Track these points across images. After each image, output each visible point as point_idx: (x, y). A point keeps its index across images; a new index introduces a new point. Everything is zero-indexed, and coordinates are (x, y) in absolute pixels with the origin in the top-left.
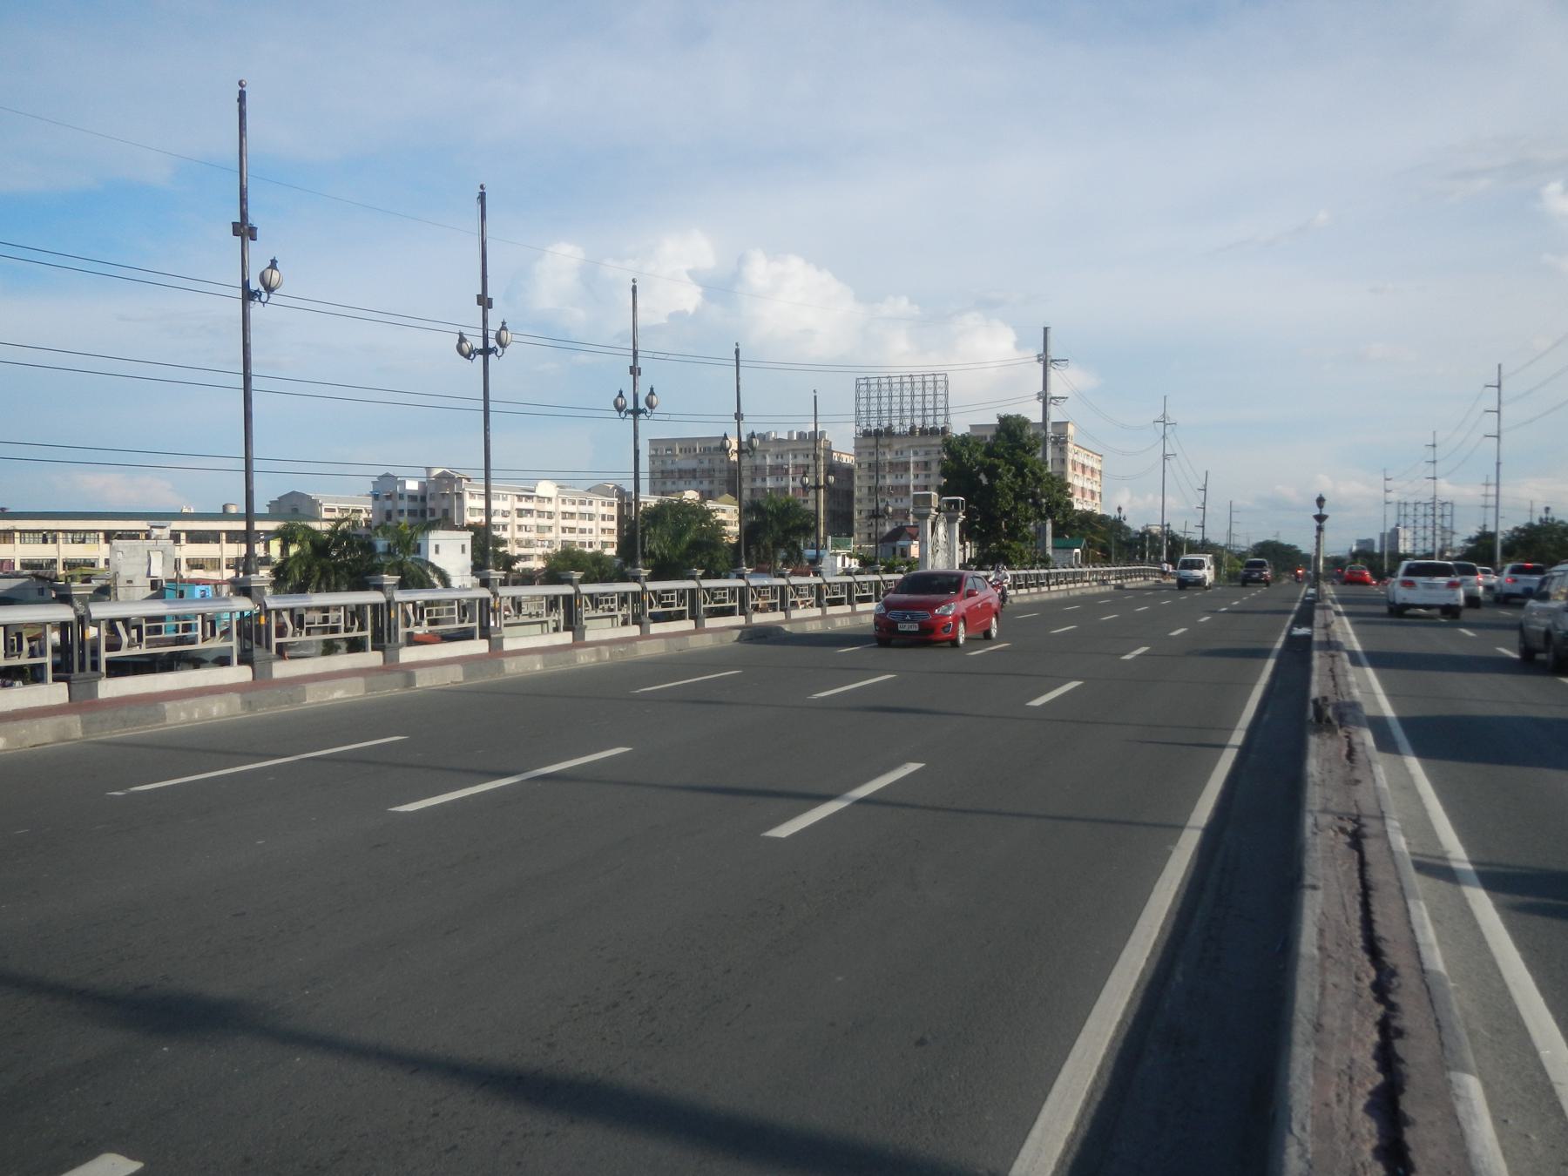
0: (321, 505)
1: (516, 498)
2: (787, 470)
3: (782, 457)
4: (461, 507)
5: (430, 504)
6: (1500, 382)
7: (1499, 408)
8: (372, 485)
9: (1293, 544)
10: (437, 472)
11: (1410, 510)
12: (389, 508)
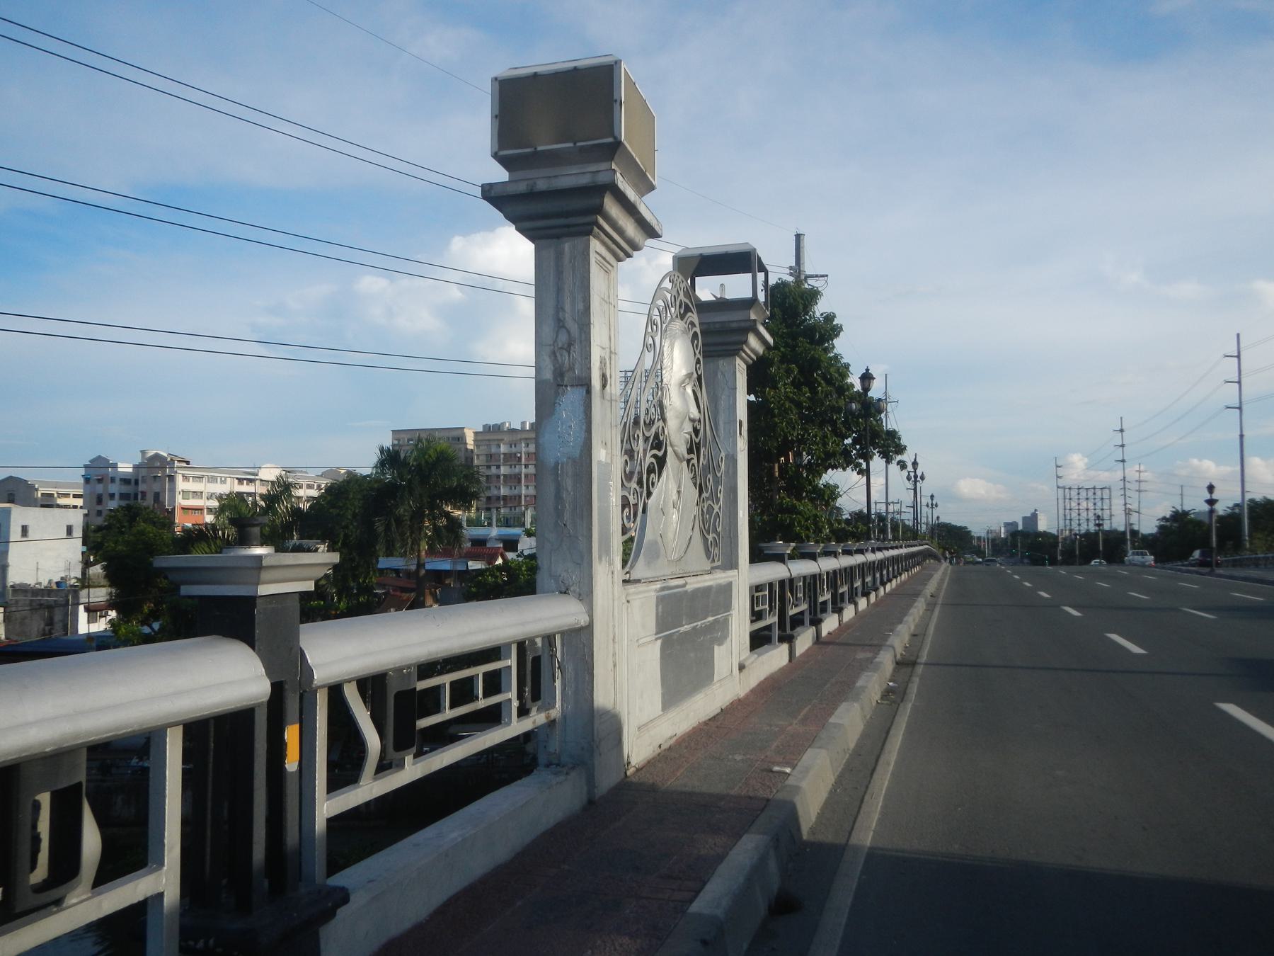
0: (37, 490)
1: (236, 481)
2: (520, 459)
3: (515, 446)
4: (173, 490)
5: (142, 487)
6: (1239, 352)
7: (1240, 378)
9: (963, 525)
10: (151, 454)
11: (1074, 493)
12: (101, 492)
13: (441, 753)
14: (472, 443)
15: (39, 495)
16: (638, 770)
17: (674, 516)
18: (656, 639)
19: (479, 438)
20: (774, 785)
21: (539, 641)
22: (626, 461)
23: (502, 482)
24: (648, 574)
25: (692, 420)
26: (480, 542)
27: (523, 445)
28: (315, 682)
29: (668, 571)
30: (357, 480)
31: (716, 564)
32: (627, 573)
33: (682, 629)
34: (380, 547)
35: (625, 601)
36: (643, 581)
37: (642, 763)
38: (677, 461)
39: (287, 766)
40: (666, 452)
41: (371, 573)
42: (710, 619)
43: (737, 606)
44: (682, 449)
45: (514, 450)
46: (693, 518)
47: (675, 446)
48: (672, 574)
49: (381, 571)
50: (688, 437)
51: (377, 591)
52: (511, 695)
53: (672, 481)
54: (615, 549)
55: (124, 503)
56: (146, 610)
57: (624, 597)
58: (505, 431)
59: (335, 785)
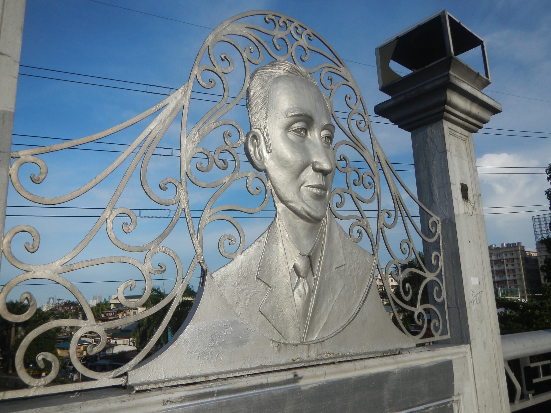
2: (503, 262)
3: (500, 256)
9: (497, 317)
23: (495, 274)
27: (504, 255)
41: (407, 322)
45: (499, 258)
47: (290, 202)
58: (493, 249)
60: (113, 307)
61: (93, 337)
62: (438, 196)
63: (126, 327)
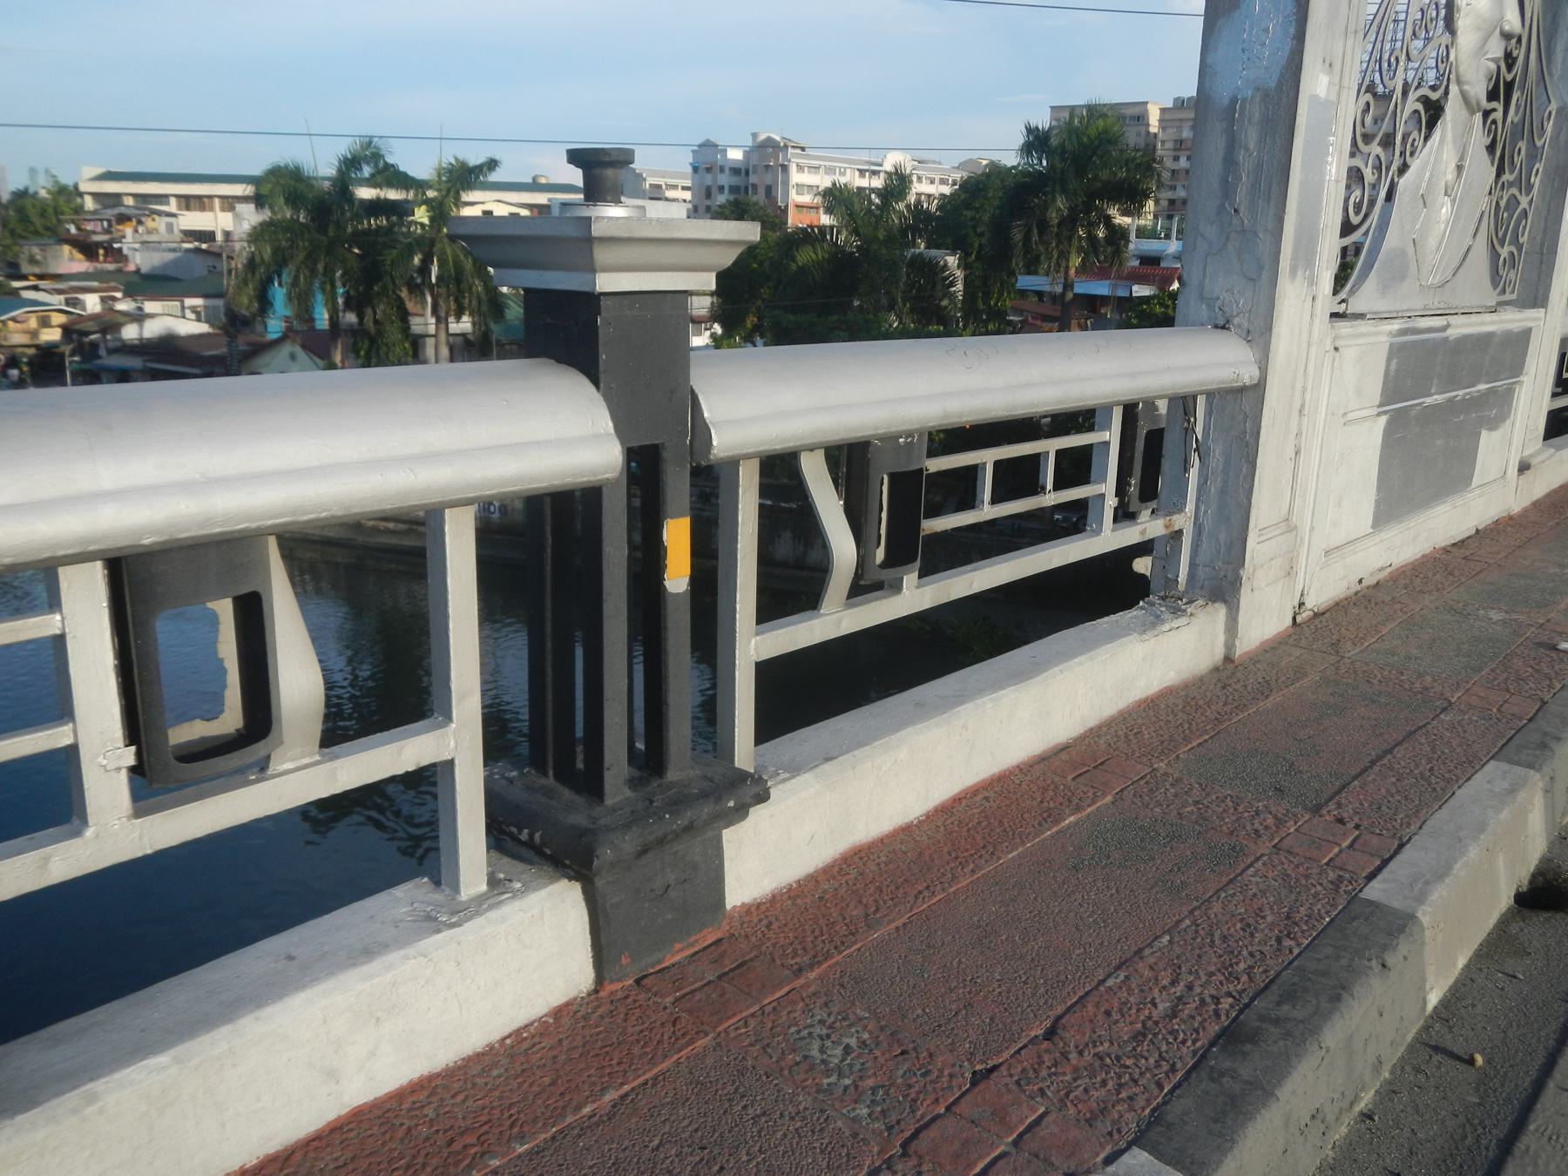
0: (645, 180)
1: (857, 173)
4: (786, 183)
5: (753, 179)
8: (691, 155)
10: (762, 137)
13: (971, 571)
14: (1157, 124)
15: (647, 186)
16: (1316, 615)
17: (1444, 210)
18: (1379, 414)
19: (1167, 117)
20: (1556, 673)
21: (1162, 406)
22: (1368, 104)
24: (1382, 306)
25: (1507, 36)
26: (1151, 261)
28: (715, 451)
29: (1417, 304)
30: (1000, 173)
31: (1508, 297)
32: (1343, 301)
33: (1429, 401)
34: (1017, 262)
35: (1329, 347)
36: (1368, 316)
37: (1326, 604)
38: (1464, 113)
39: (667, 583)
40: (1447, 92)
42: (1482, 387)
43: (1533, 371)
44: (1479, 90)
46: (1478, 215)
48: (1425, 309)
49: (1023, 293)
50: (1493, 66)
51: (1011, 318)
52: (1104, 488)
53: (1450, 146)
54: (1325, 258)
55: (731, 198)
56: (749, 325)
57: (1329, 341)
59: (772, 607)
60: (89, 204)
61: (59, 292)
62: (1559, 66)
63: (154, 268)
